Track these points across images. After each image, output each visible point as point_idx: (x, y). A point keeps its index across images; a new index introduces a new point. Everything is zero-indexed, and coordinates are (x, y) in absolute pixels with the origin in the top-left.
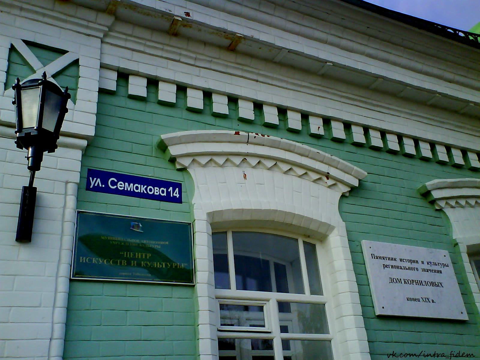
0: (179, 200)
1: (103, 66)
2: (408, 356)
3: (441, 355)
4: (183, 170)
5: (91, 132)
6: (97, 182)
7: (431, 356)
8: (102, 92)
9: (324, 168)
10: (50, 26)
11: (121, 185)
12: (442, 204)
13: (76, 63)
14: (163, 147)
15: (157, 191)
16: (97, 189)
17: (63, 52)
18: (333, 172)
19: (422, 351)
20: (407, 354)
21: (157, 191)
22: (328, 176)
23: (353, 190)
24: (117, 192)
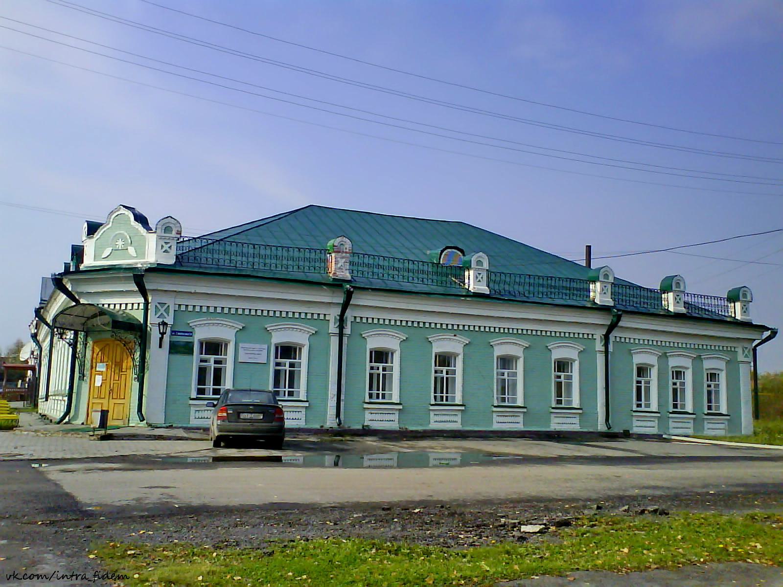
0: (192, 336)
1: (175, 304)
2: (36, 578)
3: (81, 576)
4: (193, 328)
5: (172, 324)
6: (173, 333)
7: (66, 576)
8: (175, 311)
9: (231, 324)
10: (611, 450)
11: (179, 334)
12: (271, 331)
13: (169, 306)
14: (547, 347)
15: (186, 334)
16: (174, 335)
17: (166, 303)
18: (234, 325)
19: (55, 572)
20: (34, 576)
21: (186, 334)
22: (233, 327)
23: (581, 351)
24: (177, 335)
